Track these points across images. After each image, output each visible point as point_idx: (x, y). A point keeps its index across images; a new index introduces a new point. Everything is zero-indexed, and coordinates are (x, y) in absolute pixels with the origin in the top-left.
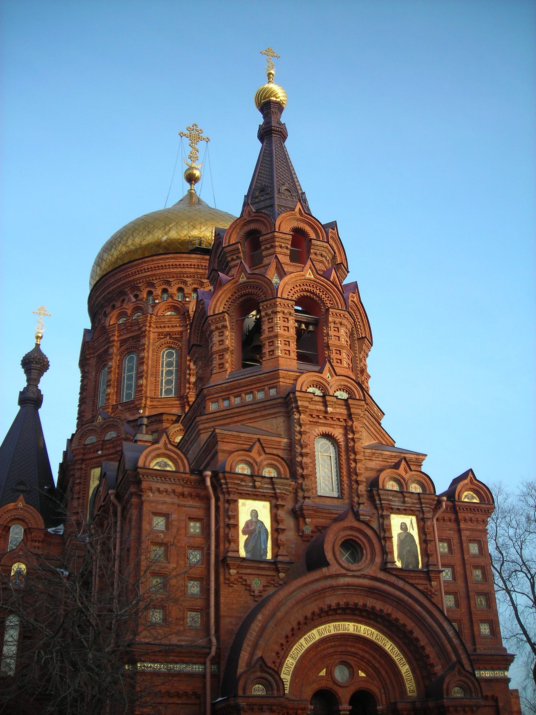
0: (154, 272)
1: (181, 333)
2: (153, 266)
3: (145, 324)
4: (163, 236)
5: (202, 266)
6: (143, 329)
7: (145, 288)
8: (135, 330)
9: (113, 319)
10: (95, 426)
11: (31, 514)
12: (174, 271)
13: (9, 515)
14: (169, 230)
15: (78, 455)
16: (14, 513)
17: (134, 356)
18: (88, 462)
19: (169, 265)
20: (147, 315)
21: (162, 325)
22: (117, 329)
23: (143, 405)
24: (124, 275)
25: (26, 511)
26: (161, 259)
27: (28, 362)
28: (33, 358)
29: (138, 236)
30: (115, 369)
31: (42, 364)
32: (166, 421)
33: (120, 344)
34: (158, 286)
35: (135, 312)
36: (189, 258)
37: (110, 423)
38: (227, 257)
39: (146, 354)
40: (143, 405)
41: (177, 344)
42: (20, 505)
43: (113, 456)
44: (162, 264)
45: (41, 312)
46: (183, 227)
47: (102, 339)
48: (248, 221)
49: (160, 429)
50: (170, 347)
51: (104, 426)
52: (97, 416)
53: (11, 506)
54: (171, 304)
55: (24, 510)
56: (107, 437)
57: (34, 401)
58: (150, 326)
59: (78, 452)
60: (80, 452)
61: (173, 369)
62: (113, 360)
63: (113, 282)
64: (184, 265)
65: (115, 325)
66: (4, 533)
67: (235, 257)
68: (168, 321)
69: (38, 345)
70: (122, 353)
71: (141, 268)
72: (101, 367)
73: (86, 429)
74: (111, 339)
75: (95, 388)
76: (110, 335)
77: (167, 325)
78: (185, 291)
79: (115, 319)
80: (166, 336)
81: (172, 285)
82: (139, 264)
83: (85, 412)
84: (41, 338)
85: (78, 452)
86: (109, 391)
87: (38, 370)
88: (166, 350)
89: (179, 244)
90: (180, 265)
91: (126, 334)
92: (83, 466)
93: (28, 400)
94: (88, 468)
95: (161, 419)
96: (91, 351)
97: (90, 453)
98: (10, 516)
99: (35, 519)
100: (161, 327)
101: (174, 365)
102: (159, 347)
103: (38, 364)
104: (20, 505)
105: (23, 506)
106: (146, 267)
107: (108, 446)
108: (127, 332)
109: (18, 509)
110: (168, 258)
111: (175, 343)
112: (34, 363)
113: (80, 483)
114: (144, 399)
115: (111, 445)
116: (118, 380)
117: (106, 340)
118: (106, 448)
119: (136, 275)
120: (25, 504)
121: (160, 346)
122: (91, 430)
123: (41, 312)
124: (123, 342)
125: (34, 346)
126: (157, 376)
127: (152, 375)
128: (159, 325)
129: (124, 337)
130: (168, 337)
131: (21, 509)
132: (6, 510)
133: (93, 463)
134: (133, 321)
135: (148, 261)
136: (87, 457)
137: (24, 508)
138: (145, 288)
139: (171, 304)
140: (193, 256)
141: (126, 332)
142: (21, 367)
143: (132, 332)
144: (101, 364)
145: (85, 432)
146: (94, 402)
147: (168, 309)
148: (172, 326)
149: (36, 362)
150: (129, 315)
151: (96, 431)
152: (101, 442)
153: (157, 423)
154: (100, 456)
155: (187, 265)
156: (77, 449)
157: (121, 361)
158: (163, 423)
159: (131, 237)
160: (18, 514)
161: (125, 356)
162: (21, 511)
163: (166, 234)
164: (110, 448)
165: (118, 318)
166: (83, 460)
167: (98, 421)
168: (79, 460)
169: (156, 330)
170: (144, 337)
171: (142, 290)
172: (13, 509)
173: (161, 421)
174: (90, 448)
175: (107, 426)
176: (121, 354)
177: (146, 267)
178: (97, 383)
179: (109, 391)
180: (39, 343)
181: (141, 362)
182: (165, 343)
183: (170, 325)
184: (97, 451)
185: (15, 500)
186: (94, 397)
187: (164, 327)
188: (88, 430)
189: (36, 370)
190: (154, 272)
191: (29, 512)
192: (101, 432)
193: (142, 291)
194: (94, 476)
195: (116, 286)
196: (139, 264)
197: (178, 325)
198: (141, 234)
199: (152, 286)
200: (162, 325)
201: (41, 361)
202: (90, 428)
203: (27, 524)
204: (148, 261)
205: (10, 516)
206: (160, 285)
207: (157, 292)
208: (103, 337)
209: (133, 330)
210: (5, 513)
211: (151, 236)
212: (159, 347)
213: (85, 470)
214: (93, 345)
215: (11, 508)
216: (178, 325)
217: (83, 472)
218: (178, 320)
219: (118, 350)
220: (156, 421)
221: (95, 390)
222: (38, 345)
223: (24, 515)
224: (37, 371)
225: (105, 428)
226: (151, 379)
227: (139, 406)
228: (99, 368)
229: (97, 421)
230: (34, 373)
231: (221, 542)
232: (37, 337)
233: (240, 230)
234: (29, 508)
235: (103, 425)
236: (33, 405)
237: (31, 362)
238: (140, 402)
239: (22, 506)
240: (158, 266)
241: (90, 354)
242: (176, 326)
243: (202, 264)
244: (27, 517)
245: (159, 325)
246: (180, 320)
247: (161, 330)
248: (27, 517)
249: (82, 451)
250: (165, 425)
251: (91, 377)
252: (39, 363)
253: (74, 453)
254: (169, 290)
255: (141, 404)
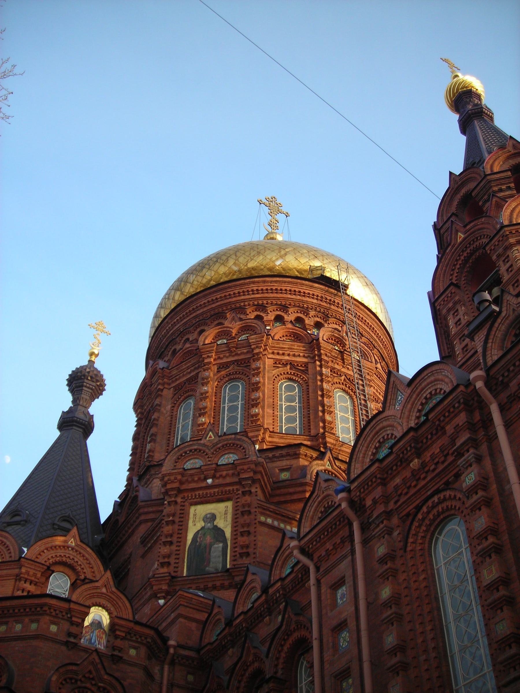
0: (266, 295)
1: (306, 365)
2: (265, 288)
3: (259, 345)
4: (277, 259)
5: (326, 299)
6: (256, 351)
7: (253, 311)
8: (243, 353)
9: (209, 338)
10: (204, 445)
11: (87, 559)
12: (292, 297)
13: (52, 553)
14: (286, 254)
15: (173, 482)
16: (60, 552)
17: (239, 384)
18: (186, 495)
19: (286, 290)
20: (262, 334)
21: (281, 352)
22: (215, 350)
23: (260, 438)
24: (223, 295)
25: (80, 553)
26: (276, 282)
27: (81, 376)
28: (89, 372)
29: (244, 256)
30: (212, 396)
31: (98, 384)
32: (304, 457)
33: (218, 369)
34: (271, 312)
35: (243, 333)
36: (312, 287)
37: (230, 442)
38: (491, 187)
39: (262, 380)
40: (260, 438)
41: (301, 376)
42: (72, 542)
43: (231, 488)
44: (276, 287)
45: (99, 327)
46: (302, 254)
47: (185, 364)
48: (513, 154)
49: (294, 466)
50: (290, 380)
51: (219, 446)
52: (207, 433)
53: (59, 540)
54: (291, 330)
55: (76, 551)
56: (223, 461)
57: (84, 425)
58: (264, 350)
59: (172, 478)
60: (176, 479)
61: (296, 404)
62: (209, 385)
63: (204, 303)
64: (304, 293)
65: (212, 345)
66: (43, 580)
67: (504, 187)
68: (289, 348)
69: (91, 362)
70: (221, 379)
71: (248, 289)
72: (181, 399)
73: (187, 449)
74: (206, 361)
75: (171, 424)
76: (203, 356)
77: (286, 352)
78: (306, 322)
79: (211, 339)
80: (285, 365)
81: (290, 313)
82: (245, 284)
83: (153, 452)
84: (97, 356)
85: (172, 478)
86: (203, 420)
87: (92, 389)
88: (285, 382)
89: (298, 271)
90: (300, 292)
91: (227, 357)
92: (179, 500)
93: (76, 422)
94: (187, 504)
95: (298, 452)
96: (165, 380)
97: (193, 481)
98: (54, 555)
99: (92, 568)
100: (278, 354)
101: (297, 401)
102: (276, 375)
103: (93, 382)
104: (72, 542)
105: (77, 545)
106: (255, 288)
107: (224, 473)
108: (230, 356)
109: (68, 547)
110: (285, 282)
111: (298, 374)
112: (89, 378)
113: (173, 522)
114: (262, 431)
115: (231, 472)
116: (214, 409)
117: (199, 362)
118: (221, 476)
119: (239, 296)
120: (79, 543)
121: (278, 375)
122: (196, 450)
123: (99, 327)
124: (221, 367)
125: (86, 363)
126: (275, 409)
127: (269, 407)
128: (276, 351)
129: (225, 360)
130: (288, 367)
131: (73, 549)
132: (50, 545)
133: (196, 496)
134: (239, 342)
135: (258, 282)
136: (184, 487)
137: (77, 548)
138: (253, 311)
139: (291, 330)
140: (316, 285)
141: (228, 355)
142: (74, 369)
143: (237, 354)
144: (181, 396)
145: (186, 453)
146: (169, 440)
147: (287, 336)
148: (294, 355)
149: (91, 377)
150: (233, 335)
151: (204, 452)
152: (214, 466)
153: (288, 457)
154: (209, 487)
155: (309, 294)
156: (170, 474)
157: (219, 388)
158: (299, 458)
159: (234, 257)
160: (67, 555)
161: (226, 383)
162: (71, 552)
163: (281, 257)
164: (227, 475)
165: (218, 336)
166: (179, 491)
167: (207, 439)
168: (172, 489)
169: (271, 356)
170: (259, 359)
171: (248, 313)
172: (60, 547)
173: (297, 456)
174: (192, 475)
175: (223, 446)
176: (220, 380)
177: (255, 288)
178: (174, 419)
179: (203, 420)
180: (93, 359)
181: (256, 387)
182: (284, 373)
183: (291, 353)
184: (206, 479)
185: (66, 532)
186: (169, 435)
187: (283, 354)
188: (191, 451)
189: (89, 388)
190: (266, 295)
191: (83, 556)
192: (213, 454)
193: (248, 315)
194: (195, 515)
195: (209, 308)
196: (245, 284)
197: (301, 354)
198: (247, 254)
199: (262, 310)
200: (281, 352)
201: (98, 378)
202: (196, 447)
203: (77, 573)
204: (258, 282)
205: (54, 555)
206: (274, 310)
207: (269, 317)
208: (190, 362)
209: (239, 352)
210: (47, 549)
211: (261, 257)
212: (276, 375)
213: (181, 506)
214: (170, 373)
215: (57, 543)
216: (301, 354)
217: (179, 507)
218: (301, 348)
219: (214, 375)
220: (288, 455)
221: (171, 426)
222: (91, 362)
223: (76, 559)
224: (90, 391)
225: (219, 448)
226: (268, 411)
227: (255, 439)
228: (177, 401)
229: (206, 438)
230: (85, 395)
231: (362, 636)
232: (92, 354)
233: (504, 163)
234: (85, 550)
235: (217, 444)
236: (81, 430)
237: (84, 375)
238: (256, 433)
239: (74, 544)
240: (272, 289)
241: (163, 384)
242: (299, 356)
243: (327, 297)
244: (79, 563)
245: (276, 351)
246: (305, 349)
247: (278, 357)
248: (79, 563)
249: (179, 477)
250: (303, 462)
251: (165, 412)
252: (94, 380)
253: (166, 479)
254: (286, 317)
255: (257, 436)
